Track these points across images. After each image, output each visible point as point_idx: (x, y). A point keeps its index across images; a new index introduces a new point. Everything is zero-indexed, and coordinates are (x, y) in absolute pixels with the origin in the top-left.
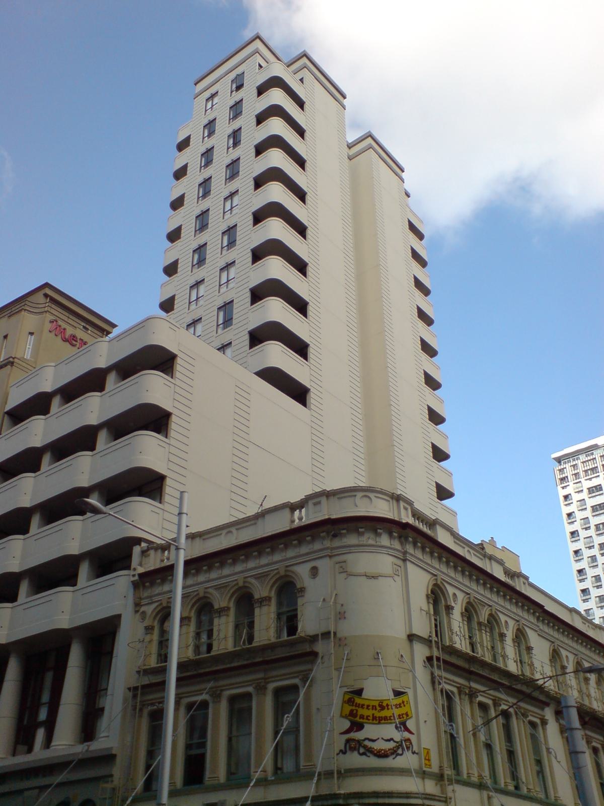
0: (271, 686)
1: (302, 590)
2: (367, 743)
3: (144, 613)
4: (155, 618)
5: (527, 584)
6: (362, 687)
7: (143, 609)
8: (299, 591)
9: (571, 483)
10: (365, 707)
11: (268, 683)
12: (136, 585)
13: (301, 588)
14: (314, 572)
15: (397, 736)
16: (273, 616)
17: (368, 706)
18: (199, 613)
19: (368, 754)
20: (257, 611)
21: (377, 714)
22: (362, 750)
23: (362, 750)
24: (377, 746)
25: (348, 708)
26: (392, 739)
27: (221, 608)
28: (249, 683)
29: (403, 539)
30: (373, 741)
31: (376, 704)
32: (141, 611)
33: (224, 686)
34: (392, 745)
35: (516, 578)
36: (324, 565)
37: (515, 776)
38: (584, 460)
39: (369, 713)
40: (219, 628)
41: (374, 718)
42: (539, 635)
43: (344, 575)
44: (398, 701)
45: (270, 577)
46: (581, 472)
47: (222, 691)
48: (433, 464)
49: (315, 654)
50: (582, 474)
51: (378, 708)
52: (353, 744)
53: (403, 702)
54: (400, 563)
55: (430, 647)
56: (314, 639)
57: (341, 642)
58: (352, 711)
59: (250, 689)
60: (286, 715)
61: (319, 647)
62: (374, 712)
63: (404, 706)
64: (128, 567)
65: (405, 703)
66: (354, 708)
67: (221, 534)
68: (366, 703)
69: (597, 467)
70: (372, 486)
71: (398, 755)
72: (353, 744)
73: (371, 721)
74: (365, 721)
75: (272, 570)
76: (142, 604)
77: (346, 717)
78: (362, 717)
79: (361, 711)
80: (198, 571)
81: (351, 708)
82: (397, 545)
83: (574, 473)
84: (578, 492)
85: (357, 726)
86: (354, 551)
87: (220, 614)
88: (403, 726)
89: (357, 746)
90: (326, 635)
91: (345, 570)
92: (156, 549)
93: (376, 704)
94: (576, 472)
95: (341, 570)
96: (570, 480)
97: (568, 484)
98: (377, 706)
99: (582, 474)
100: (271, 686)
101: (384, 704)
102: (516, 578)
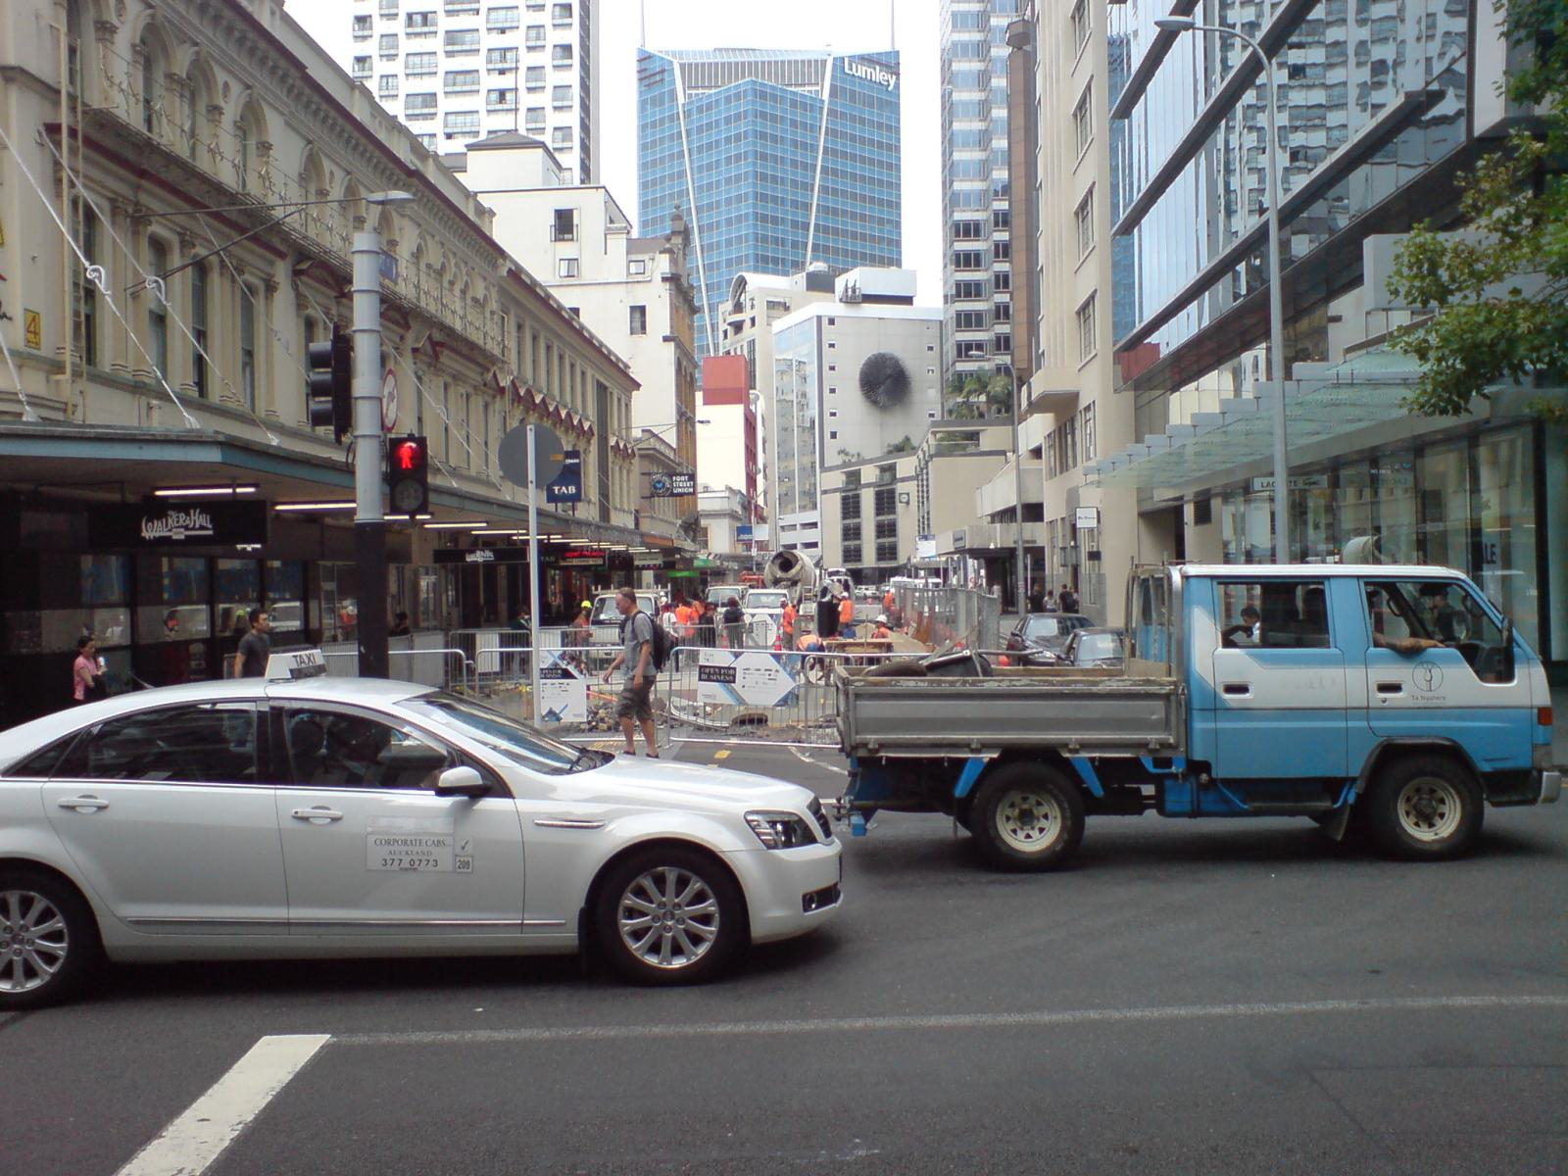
42: (287, 123)
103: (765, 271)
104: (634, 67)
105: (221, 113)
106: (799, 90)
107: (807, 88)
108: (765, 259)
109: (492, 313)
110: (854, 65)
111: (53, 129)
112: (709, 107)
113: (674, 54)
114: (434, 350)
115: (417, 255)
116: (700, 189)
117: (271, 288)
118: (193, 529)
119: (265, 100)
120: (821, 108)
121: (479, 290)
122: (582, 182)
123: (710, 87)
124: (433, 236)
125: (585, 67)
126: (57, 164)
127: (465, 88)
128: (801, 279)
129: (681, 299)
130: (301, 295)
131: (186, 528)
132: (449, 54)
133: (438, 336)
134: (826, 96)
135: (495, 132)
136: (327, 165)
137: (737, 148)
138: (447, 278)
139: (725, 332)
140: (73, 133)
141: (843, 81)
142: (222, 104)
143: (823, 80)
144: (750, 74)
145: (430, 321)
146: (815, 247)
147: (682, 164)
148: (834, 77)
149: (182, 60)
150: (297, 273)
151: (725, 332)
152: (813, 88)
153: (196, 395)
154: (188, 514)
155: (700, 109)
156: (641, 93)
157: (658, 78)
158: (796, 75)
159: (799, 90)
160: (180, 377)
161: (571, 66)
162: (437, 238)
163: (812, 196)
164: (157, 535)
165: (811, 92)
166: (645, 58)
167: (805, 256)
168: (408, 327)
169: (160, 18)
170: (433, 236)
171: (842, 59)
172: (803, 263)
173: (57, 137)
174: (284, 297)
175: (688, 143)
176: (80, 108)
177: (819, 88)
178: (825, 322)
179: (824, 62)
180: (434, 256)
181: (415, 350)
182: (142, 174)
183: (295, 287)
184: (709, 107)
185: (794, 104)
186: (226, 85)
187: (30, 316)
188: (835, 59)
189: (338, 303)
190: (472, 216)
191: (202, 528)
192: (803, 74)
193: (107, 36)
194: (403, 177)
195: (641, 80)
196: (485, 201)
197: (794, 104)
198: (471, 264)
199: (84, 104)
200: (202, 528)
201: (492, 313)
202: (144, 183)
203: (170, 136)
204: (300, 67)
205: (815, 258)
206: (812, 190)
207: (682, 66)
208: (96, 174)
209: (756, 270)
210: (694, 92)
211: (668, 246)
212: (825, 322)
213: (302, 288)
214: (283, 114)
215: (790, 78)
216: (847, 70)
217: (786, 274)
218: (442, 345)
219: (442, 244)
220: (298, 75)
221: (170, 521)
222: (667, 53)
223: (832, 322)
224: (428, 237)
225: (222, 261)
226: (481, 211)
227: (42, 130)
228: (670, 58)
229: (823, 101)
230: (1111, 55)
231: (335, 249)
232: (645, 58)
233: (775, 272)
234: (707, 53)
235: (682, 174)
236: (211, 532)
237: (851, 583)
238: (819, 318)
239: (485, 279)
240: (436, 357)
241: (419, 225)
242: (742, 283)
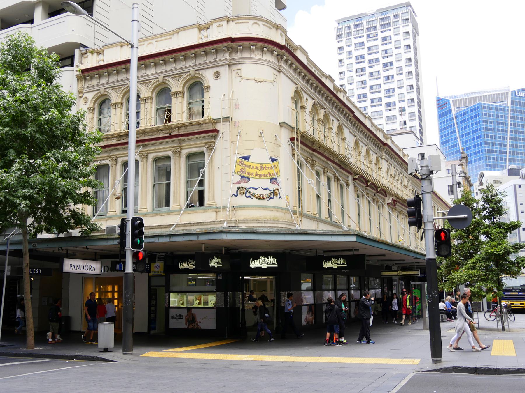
0: (151, 156)
1: (208, 88)
2: (251, 190)
3: (86, 98)
4: (95, 102)
5: (345, 97)
6: (249, 154)
7: (85, 95)
8: (206, 88)
9: (344, 39)
10: (251, 167)
11: (182, 149)
12: (79, 79)
13: (207, 86)
14: (217, 75)
15: (272, 187)
16: (154, 110)
17: (253, 167)
18: (190, 88)
19: (252, 197)
20: (173, 100)
21: (259, 172)
22: (248, 194)
23: (248, 194)
24: (258, 192)
25: (239, 168)
26: (267, 189)
27: (146, 97)
28: (169, 149)
29: (279, 57)
30: (256, 189)
31: (258, 165)
32: (84, 96)
33: (149, 150)
34: (267, 192)
35: (339, 92)
36: (224, 71)
37: (330, 214)
38: (404, 12)
39: (254, 171)
40: (83, 124)
41: (257, 175)
42: (349, 131)
43: (239, 79)
44: (273, 164)
45: (152, 83)
46: (401, 20)
47: (148, 153)
48: (275, 12)
49: (217, 131)
50: (379, 27)
51: (260, 169)
52: (242, 190)
53: (275, 165)
54: (277, 73)
55: (292, 131)
56: (216, 122)
57: (236, 125)
58: (242, 169)
59: (170, 153)
60: (201, 170)
61: (219, 127)
62: (257, 171)
63: (276, 168)
64: (72, 65)
65: (277, 166)
66: (243, 168)
67: (144, 44)
68: (252, 165)
69: (343, 34)
70: (169, 40)
71: (271, 198)
72: (242, 190)
73: (255, 177)
74: (250, 176)
75: (184, 73)
76: (84, 92)
77: (238, 173)
78: (248, 173)
79: (248, 170)
80: (146, 67)
81: (241, 167)
82: (274, 60)
83: (347, 32)
84: (349, 46)
85: (245, 178)
86: (242, 62)
87: (145, 101)
88: (273, 180)
89: (245, 192)
90: (226, 119)
91: (239, 75)
92: (92, 53)
93: (258, 165)
94: (349, 31)
95: (237, 75)
96: (392, 26)
97: (342, 39)
98: (259, 167)
99: (352, 33)
100: (185, 152)
101: (264, 166)
102: (339, 92)
103: (490, 170)
104: (435, 103)
105: (332, 130)
106: (498, 104)
107: (502, 103)
108: (490, 166)
109: (410, 190)
110: (519, 93)
111: (292, 139)
112: (464, 114)
113: (450, 97)
114: (394, 203)
115: (387, 172)
116: (463, 143)
117: (348, 185)
118: (340, 264)
119: (344, 125)
120: (508, 110)
121: (406, 182)
122: (421, 144)
123: (464, 107)
124: (391, 165)
125: (419, 106)
126: (293, 150)
127: (378, 117)
128: (506, 171)
129: (466, 182)
130: (356, 187)
131: (338, 264)
132: (372, 106)
133: (395, 199)
134: (509, 105)
135: (389, 130)
136: (361, 144)
137: (448, 131)
138: (396, 178)
139: (477, 193)
140: (297, 139)
141: (516, 99)
142: (333, 127)
143: (508, 99)
144: (479, 101)
145: (392, 194)
146: (510, 160)
147: (456, 135)
148: (512, 98)
149: (322, 112)
150: (354, 179)
151: (477, 193)
152: (504, 103)
153: (330, 220)
154: (338, 259)
155: (461, 115)
156: (439, 112)
157: (444, 106)
158: (497, 99)
159: (498, 104)
160: (325, 215)
161: (414, 105)
162: (393, 165)
163: (507, 141)
164: (328, 266)
165: (503, 104)
166: (439, 100)
167: (506, 163)
168: (386, 196)
169: (316, 102)
170: (391, 165)
171: (515, 91)
172: (506, 166)
173: (293, 141)
174: (351, 187)
175: (458, 127)
176: (299, 132)
177: (506, 102)
178: (517, 187)
179: (507, 93)
180: (392, 171)
181: (388, 204)
182: (314, 150)
183: (354, 184)
184: (464, 114)
185: (497, 109)
186: (333, 120)
187: (287, 196)
188: (512, 91)
189: (366, 189)
190: (401, 156)
191: (343, 264)
192: (500, 98)
193: (304, 110)
194: (382, 145)
195: (438, 107)
196: (405, 151)
197: (497, 109)
198: (403, 173)
199: (300, 131)
200: (343, 264)
201: (410, 190)
202: (315, 153)
203: (319, 137)
204: (353, 112)
205: (510, 164)
206: (507, 139)
207: (453, 101)
208: (302, 153)
209: (487, 170)
210: (458, 109)
211: (461, 163)
212: (517, 187)
213: (356, 185)
214: (348, 128)
215: (495, 100)
216: (517, 95)
217: (499, 170)
218: (396, 201)
219: (394, 167)
220: (352, 115)
221: (332, 262)
222: (447, 97)
223: (520, 186)
224: (390, 166)
225: (335, 175)
226: (404, 155)
227: (289, 140)
228: (449, 99)
229: (508, 107)
230: (438, 104)
231: (366, 171)
232: (439, 100)
233: (494, 170)
234: (462, 95)
235: (456, 138)
236: (346, 265)
237: (6, 170)
238: (515, 186)
239: (407, 178)
240: (395, 205)
241: (387, 161)
242: (482, 175)
